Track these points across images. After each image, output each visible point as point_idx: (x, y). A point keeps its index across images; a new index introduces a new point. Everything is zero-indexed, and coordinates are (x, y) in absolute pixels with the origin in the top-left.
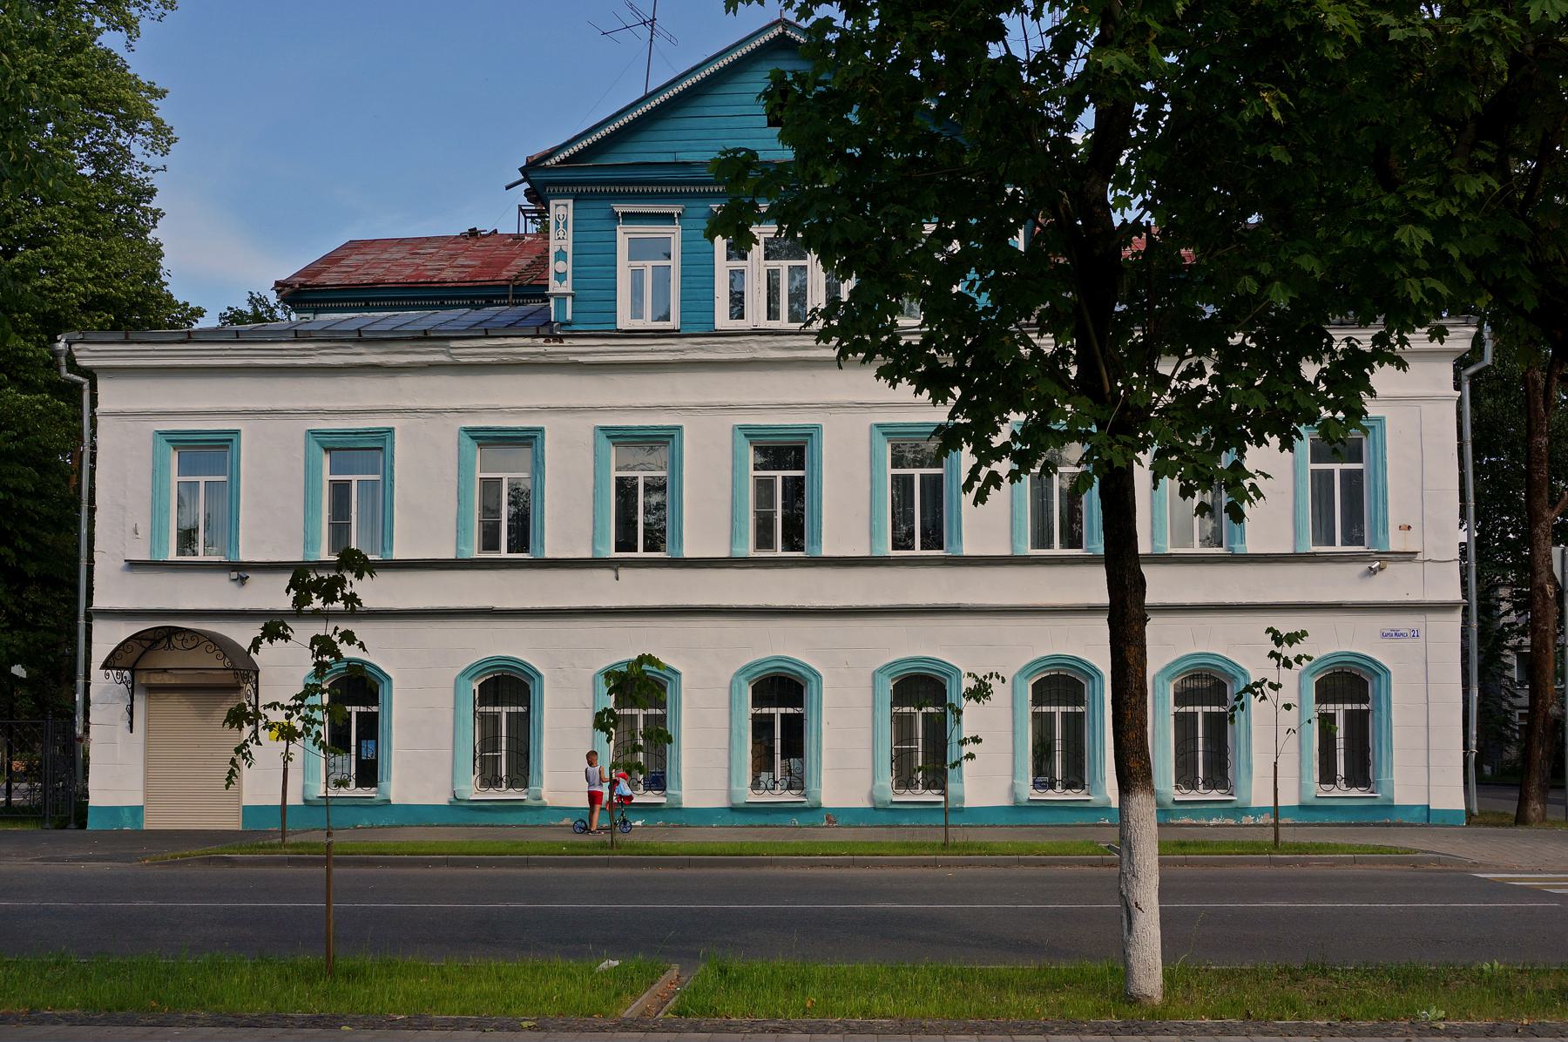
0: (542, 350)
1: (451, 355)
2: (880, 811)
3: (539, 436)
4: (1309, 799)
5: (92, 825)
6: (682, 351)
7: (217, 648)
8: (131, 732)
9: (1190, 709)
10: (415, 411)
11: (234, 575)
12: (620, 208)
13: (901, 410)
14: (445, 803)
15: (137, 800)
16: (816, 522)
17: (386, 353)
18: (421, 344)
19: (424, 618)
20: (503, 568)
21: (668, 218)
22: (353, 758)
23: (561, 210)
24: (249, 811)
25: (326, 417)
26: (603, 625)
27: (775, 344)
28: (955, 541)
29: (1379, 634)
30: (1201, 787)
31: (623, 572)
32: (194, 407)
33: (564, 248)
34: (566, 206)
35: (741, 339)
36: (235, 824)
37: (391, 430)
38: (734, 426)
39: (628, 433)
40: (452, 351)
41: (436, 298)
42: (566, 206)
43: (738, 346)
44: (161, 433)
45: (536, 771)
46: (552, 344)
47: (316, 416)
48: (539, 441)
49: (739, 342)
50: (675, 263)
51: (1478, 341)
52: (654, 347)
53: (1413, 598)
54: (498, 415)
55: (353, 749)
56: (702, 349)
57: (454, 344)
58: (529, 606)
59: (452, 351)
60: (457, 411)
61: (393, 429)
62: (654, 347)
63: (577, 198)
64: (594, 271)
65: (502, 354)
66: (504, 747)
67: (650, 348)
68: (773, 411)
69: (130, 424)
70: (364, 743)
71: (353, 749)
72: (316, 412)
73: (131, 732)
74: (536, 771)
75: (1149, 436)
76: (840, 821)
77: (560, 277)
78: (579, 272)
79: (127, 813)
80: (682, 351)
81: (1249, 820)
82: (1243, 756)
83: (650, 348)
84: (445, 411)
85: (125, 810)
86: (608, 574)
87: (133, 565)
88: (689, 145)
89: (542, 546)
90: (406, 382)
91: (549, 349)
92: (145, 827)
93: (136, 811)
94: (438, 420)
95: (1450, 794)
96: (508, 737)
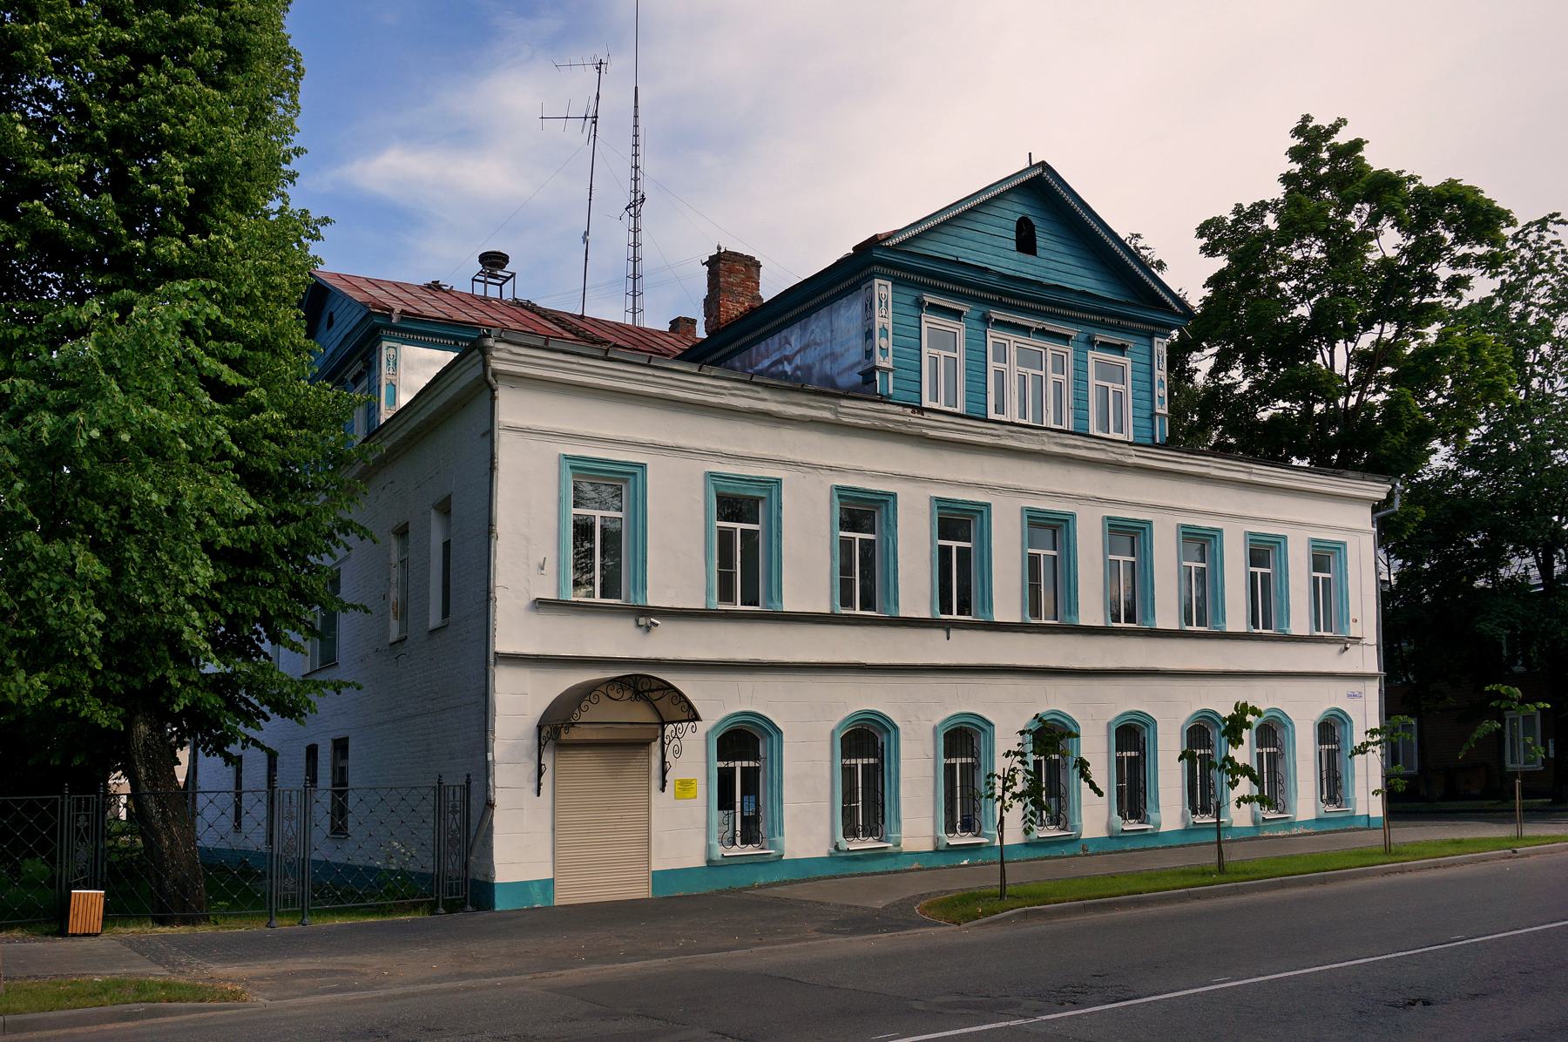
0: (907, 419)
1: (836, 413)
2: (1114, 836)
3: (891, 500)
4: (1322, 814)
5: (501, 904)
6: (999, 436)
7: (587, 698)
8: (539, 795)
9: (731, 765)
10: (796, 464)
11: (642, 621)
12: (929, 298)
13: (1118, 506)
14: (824, 854)
15: (546, 873)
16: (1072, 594)
17: (784, 403)
18: (818, 398)
19: (842, 672)
20: (867, 625)
21: (957, 315)
22: (738, 815)
23: (883, 291)
24: (661, 877)
25: (722, 460)
26: (939, 680)
27: (1058, 440)
28: (1150, 617)
29: (340, 734)
30: (958, 830)
31: (953, 633)
32: (561, 427)
33: (886, 326)
34: (887, 286)
35: (1040, 432)
36: (642, 891)
37: (778, 482)
38: (1022, 508)
39: (953, 505)
40: (840, 410)
41: (451, 337)
42: (887, 286)
43: (1036, 438)
44: (567, 457)
45: (893, 818)
46: (916, 415)
47: (714, 459)
48: (891, 507)
49: (1037, 435)
50: (960, 355)
51: (1390, 495)
52: (984, 430)
53: (1360, 670)
54: (861, 477)
55: (738, 805)
56: (1012, 437)
57: (844, 402)
58: (886, 662)
59: (840, 410)
60: (830, 468)
61: (781, 480)
62: (984, 430)
63: (897, 282)
64: (903, 352)
65: (876, 418)
66: (860, 799)
67: (979, 430)
68: (1044, 498)
69: (535, 444)
70: (746, 798)
71: (738, 805)
72: (714, 454)
73: (539, 795)
74: (893, 818)
75: (1481, 543)
76: (1091, 850)
77: (884, 351)
78: (898, 351)
79: (536, 889)
80: (999, 436)
81: (1295, 831)
82: (1293, 785)
83: (979, 430)
84: (822, 467)
85: (536, 884)
86: (941, 634)
87: (541, 604)
88: (966, 253)
89: (897, 604)
90: (789, 435)
91: (913, 420)
92: (556, 903)
93: (547, 885)
94: (814, 477)
95: (1376, 808)
96: (961, 786)
